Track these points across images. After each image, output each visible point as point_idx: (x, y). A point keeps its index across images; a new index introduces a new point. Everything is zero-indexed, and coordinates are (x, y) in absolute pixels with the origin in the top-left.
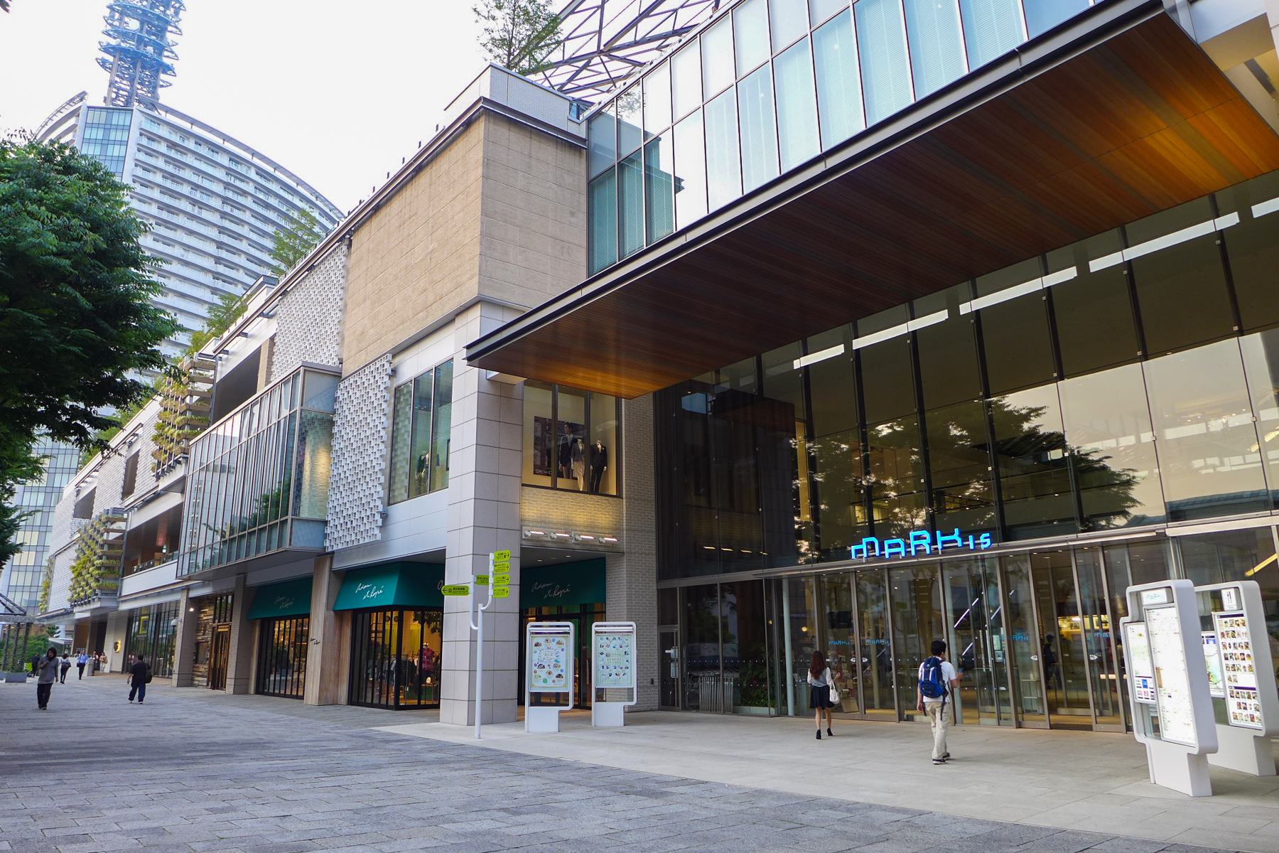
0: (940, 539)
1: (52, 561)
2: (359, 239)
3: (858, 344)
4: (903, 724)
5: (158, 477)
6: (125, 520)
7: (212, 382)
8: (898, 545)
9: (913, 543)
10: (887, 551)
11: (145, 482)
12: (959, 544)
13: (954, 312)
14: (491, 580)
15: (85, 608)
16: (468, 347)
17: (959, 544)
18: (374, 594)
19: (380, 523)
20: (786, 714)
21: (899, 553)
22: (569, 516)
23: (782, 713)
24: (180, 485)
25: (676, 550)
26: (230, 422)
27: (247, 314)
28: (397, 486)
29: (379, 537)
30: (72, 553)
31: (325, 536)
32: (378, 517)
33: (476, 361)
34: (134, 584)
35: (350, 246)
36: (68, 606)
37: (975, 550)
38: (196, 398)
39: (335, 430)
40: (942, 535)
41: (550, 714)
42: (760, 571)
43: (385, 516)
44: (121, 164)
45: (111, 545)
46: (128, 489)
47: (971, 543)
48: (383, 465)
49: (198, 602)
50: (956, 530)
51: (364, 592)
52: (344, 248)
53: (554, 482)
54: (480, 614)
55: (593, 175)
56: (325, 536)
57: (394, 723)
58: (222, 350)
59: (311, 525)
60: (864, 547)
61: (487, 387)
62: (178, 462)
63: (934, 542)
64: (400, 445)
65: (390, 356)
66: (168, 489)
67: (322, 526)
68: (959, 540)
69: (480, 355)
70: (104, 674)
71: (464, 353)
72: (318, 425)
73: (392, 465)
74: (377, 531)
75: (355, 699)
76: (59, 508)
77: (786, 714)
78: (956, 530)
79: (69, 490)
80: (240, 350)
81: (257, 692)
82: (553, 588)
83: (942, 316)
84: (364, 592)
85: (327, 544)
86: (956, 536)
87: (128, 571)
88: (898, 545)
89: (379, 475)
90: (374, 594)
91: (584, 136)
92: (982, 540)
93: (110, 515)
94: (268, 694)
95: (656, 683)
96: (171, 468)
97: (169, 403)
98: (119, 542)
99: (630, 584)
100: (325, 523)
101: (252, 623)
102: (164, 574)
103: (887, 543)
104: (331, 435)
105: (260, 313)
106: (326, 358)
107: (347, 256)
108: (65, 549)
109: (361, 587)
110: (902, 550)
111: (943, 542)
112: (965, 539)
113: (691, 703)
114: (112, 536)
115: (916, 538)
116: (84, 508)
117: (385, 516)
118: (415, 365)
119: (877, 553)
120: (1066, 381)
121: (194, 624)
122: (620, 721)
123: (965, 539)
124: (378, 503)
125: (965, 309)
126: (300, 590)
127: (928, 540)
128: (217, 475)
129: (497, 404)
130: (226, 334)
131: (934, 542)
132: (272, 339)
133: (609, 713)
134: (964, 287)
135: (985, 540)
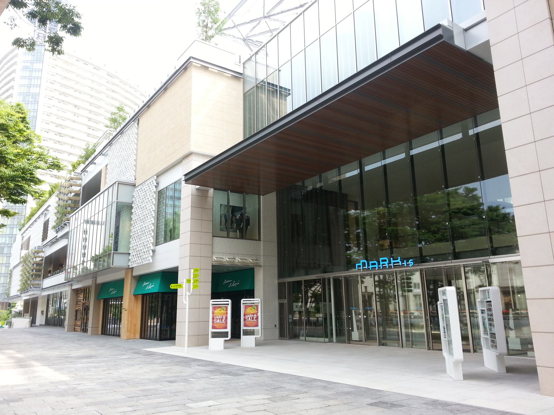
0: (392, 261)
1: (11, 271)
2: (143, 120)
3: (414, 152)
4: (381, 347)
5: (57, 232)
6: (43, 252)
7: (80, 186)
8: (375, 264)
9: (381, 263)
10: (371, 267)
11: (51, 234)
12: (400, 264)
13: (465, 134)
14: (192, 281)
15: (26, 294)
16: (185, 175)
17: (400, 264)
18: (150, 287)
19: (151, 254)
20: (333, 342)
21: (375, 267)
22: (231, 252)
23: (331, 341)
24: (66, 236)
25: (287, 264)
26: (90, 204)
27: (96, 153)
28: (160, 237)
29: (151, 261)
30: (20, 268)
31: (129, 260)
32: (151, 251)
33: (190, 181)
34: (49, 282)
35: (138, 124)
36: (19, 293)
37: (407, 266)
38: (73, 194)
39: (133, 211)
40: (393, 260)
41: (221, 341)
42: (320, 275)
43: (154, 251)
44: (40, 73)
45: (38, 264)
46: (45, 237)
47: (405, 263)
48: (153, 228)
49: (76, 292)
50: (399, 258)
51: (146, 286)
52: (136, 124)
53: (228, 234)
54: (187, 296)
55: (246, 90)
56: (129, 260)
57: (156, 346)
58: (84, 170)
59: (123, 255)
60: (361, 264)
61: (195, 192)
62: (65, 225)
63: (390, 263)
64: (161, 218)
65: (155, 177)
66: (62, 237)
67: (128, 255)
68: (400, 262)
69: (190, 178)
70: (37, 326)
71: (183, 178)
72: (123, 210)
73: (158, 227)
74: (150, 258)
75: (143, 336)
76: (14, 245)
77: (333, 342)
78: (399, 258)
79: (19, 238)
80: (92, 171)
81: (102, 334)
82: (232, 282)
83: (459, 136)
84: (146, 286)
85: (130, 264)
86: (399, 261)
87: (45, 277)
88: (375, 264)
89: (151, 232)
90: (150, 287)
91: (242, 72)
92: (410, 262)
93: (36, 250)
94: (107, 335)
95: (277, 326)
96: (63, 227)
97: (61, 196)
98: (41, 262)
99: (265, 283)
100: (129, 254)
101: (99, 300)
102: (59, 278)
103: (370, 263)
104: (132, 213)
105: (100, 153)
106: (129, 177)
107: (138, 128)
108: (17, 265)
109: (145, 284)
110: (376, 266)
111: (394, 263)
112: (403, 262)
113: (294, 336)
114: (38, 259)
115: (383, 261)
116: (26, 245)
117: (154, 251)
118: (166, 181)
119: (366, 267)
120: (486, 181)
121: (75, 302)
122: (253, 344)
123: (403, 262)
124: (151, 245)
125: (471, 132)
126: (119, 284)
127: (387, 262)
128: (96, 226)
129: (200, 200)
130: (87, 163)
131: (390, 263)
132: (106, 166)
133: (247, 341)
134: (470, 121)
135: (411, 262)
